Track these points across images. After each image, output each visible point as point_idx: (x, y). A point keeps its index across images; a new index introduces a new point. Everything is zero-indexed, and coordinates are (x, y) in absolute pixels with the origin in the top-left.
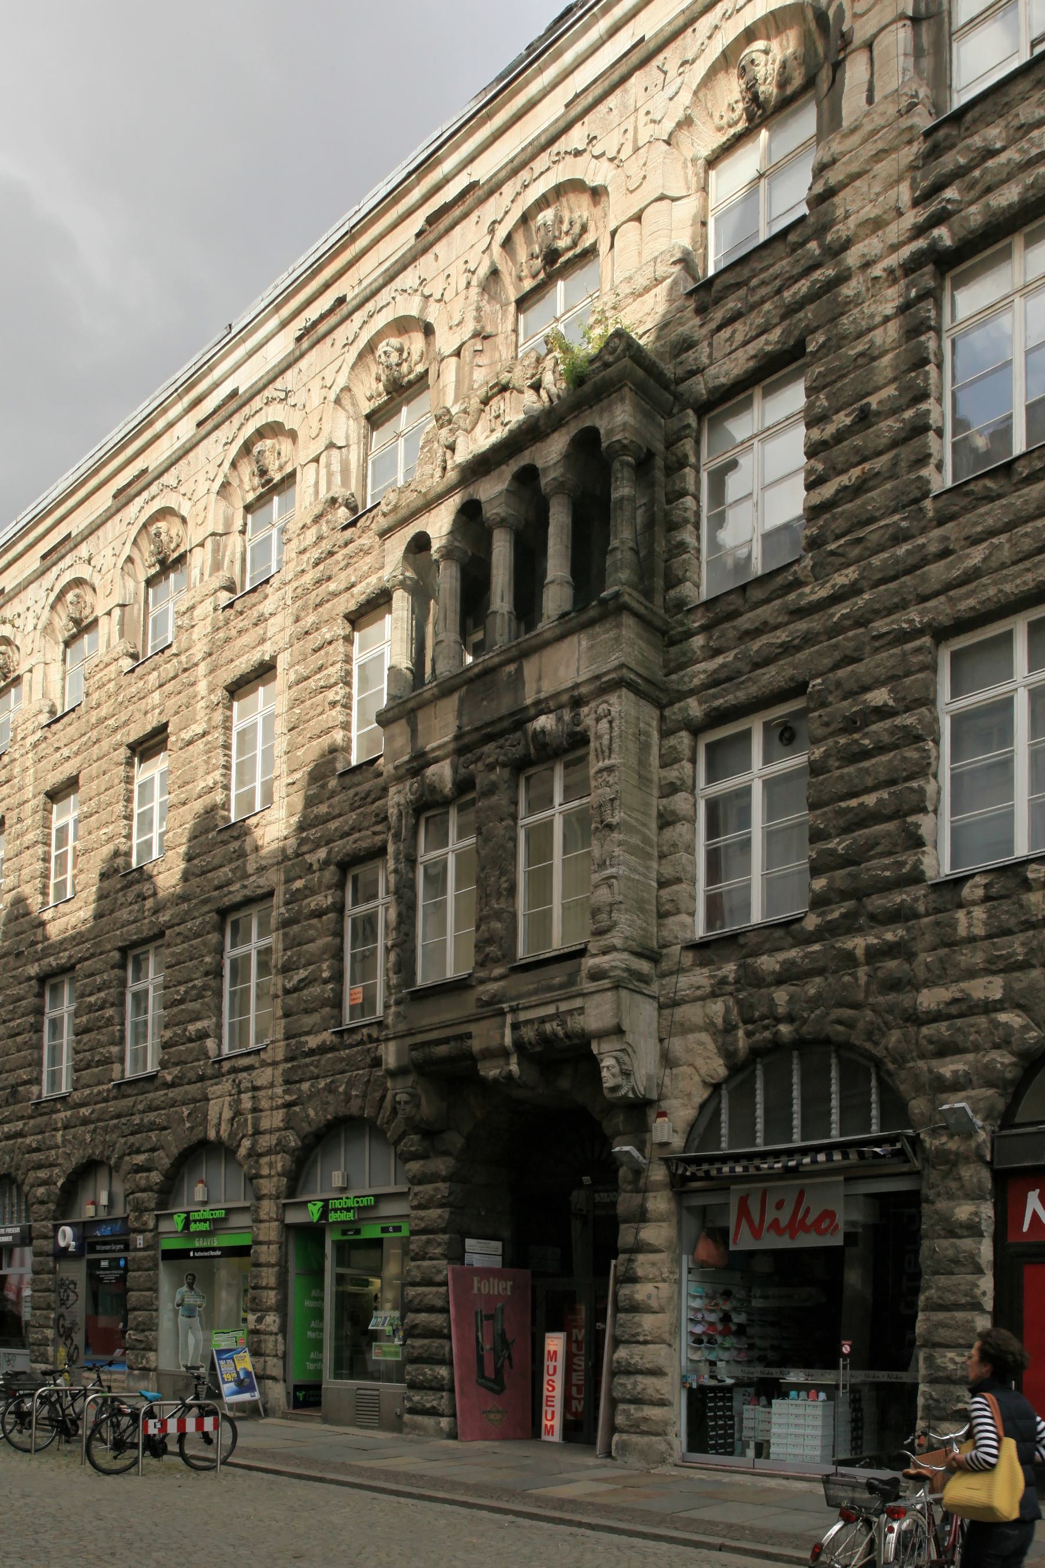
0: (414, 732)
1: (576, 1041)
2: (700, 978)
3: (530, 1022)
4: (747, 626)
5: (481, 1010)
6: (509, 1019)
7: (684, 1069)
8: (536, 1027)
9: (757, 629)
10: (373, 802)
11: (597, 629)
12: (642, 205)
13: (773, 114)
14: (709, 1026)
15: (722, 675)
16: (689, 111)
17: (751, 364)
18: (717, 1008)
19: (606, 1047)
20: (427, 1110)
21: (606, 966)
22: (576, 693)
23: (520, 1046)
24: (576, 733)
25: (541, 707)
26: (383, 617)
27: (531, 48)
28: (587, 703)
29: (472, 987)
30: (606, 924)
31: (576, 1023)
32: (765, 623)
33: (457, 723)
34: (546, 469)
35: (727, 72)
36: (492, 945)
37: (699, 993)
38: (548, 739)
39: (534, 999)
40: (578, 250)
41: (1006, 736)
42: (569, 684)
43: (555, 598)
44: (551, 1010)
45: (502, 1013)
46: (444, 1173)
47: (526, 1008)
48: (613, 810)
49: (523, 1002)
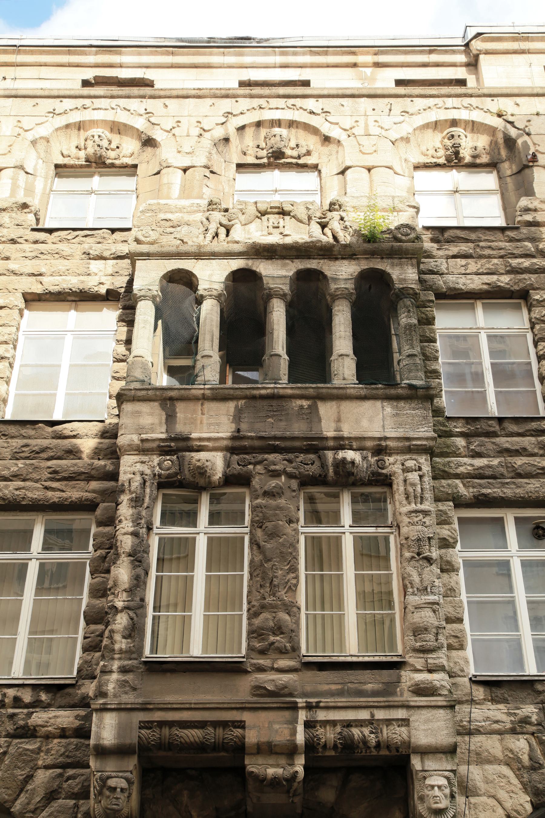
0: (171, 418)
1: (384, 752)
2: (499, 713)
3: (333, 723)
4: (507, 445)
5: (255, 699)
6: (302, 716)
8: (338, 729)
9: (517, 451)
10: (48, 459)
11: (402, 404)
12: (376, 164)
13: (463, 166)
14: (512, 761)
15: (488, 472)
16: (409, 136)
17: (485, 287)
18: (521, 745)
19: (431, 764)
22: (383, 443)
23: (311, 747)
24: (380, 474)
25: (341, 443)
26: (69, 310)
27: (210, 40)
28: (390, 455)
29: (246, 672)
30: (432, 644)
31: (396, 734)
32: (525, 449)
33: (233, 427)
34: (335, 280)
35: (434, 131)
36: (271, 636)
37: (496, 726)
38: (355, 471)
39: (342, 701)
40: (301, 161)
42: (377, 435)
43: (344, 367)
44: (364, 715)
45: (294, 707)
47: (327, 708)
48: (430, 546)
49: (325, 701)
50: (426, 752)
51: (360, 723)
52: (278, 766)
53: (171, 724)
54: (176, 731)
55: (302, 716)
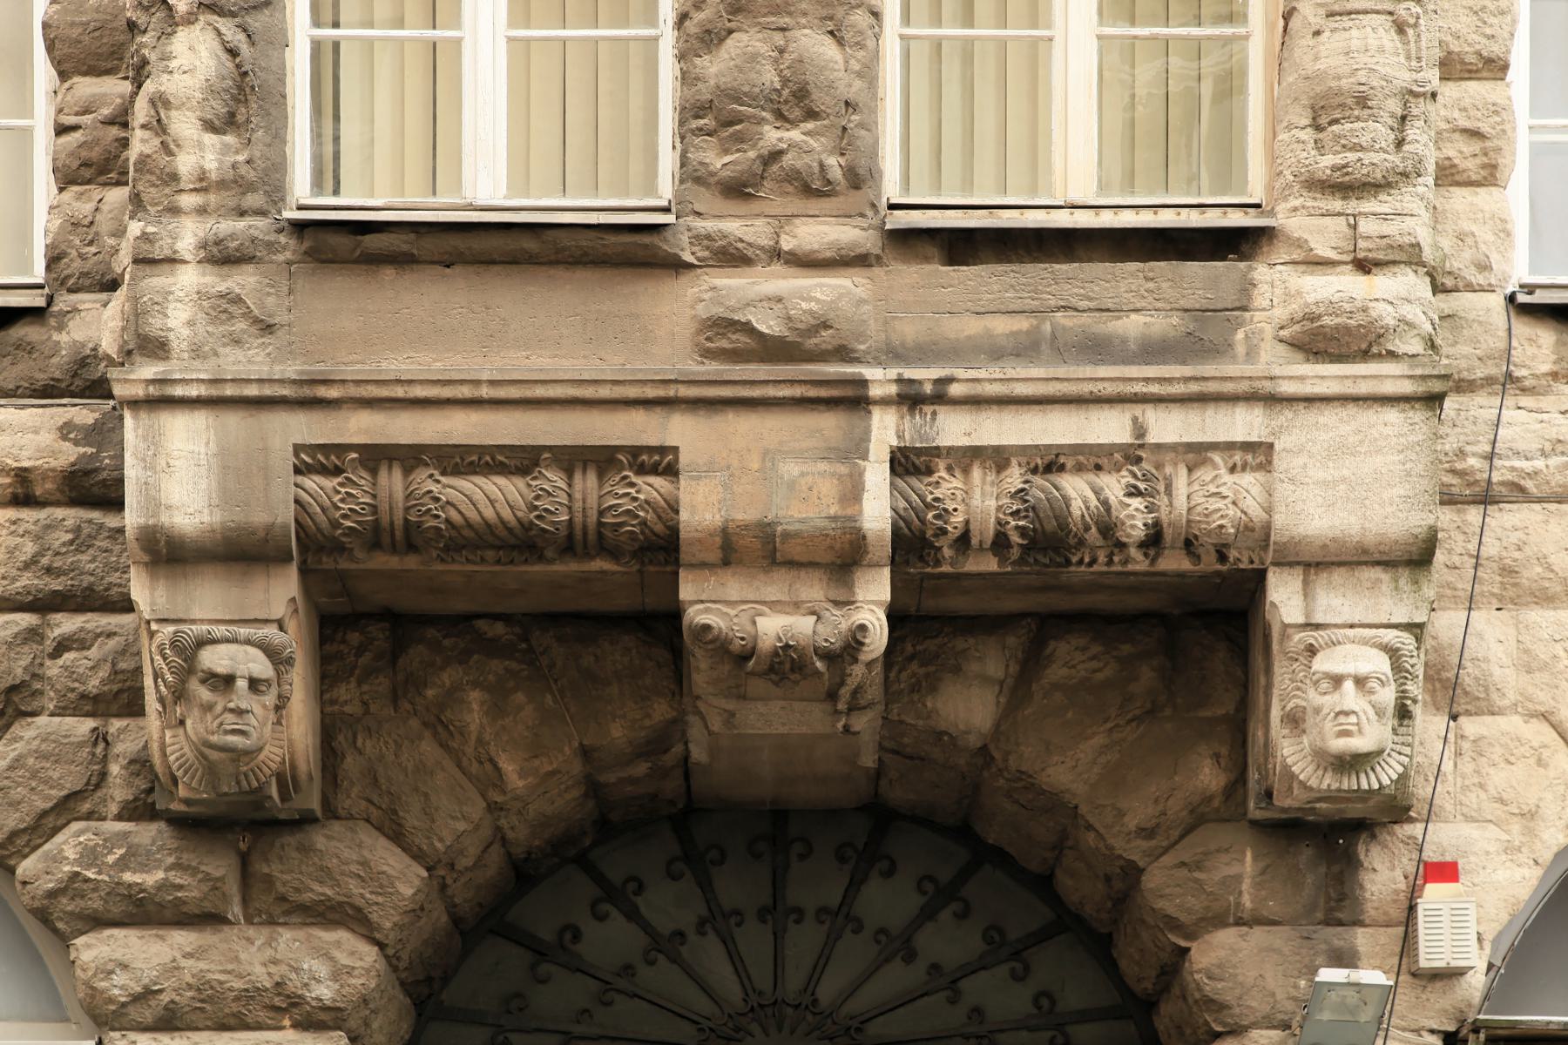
1: (1174, 562)
5: (712, 368)
6: (886, 430)
7: (1511, 723)
8: (1014, 478)
19: (1338, 601)
20: (279, 727)
21: (1386, 315)
23: (912, 544)
30: (1381, 160)
31: (1217, 499)
39: (1029, 376)
41: (932, 26)
44: (1109, 428)
45: (855, 400)
46: (325, 992)
47: (976, 402)
50: (1318, 562)
51: (1094, 459)
52: (796, 606)
53: (411, 457)
54: (427, 482)
55: (886, 430)
